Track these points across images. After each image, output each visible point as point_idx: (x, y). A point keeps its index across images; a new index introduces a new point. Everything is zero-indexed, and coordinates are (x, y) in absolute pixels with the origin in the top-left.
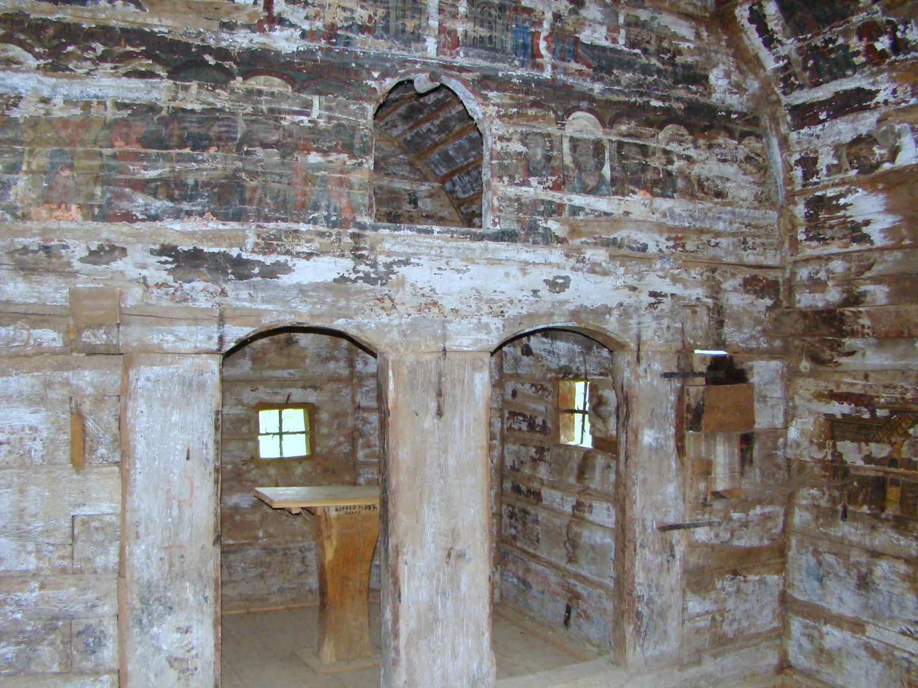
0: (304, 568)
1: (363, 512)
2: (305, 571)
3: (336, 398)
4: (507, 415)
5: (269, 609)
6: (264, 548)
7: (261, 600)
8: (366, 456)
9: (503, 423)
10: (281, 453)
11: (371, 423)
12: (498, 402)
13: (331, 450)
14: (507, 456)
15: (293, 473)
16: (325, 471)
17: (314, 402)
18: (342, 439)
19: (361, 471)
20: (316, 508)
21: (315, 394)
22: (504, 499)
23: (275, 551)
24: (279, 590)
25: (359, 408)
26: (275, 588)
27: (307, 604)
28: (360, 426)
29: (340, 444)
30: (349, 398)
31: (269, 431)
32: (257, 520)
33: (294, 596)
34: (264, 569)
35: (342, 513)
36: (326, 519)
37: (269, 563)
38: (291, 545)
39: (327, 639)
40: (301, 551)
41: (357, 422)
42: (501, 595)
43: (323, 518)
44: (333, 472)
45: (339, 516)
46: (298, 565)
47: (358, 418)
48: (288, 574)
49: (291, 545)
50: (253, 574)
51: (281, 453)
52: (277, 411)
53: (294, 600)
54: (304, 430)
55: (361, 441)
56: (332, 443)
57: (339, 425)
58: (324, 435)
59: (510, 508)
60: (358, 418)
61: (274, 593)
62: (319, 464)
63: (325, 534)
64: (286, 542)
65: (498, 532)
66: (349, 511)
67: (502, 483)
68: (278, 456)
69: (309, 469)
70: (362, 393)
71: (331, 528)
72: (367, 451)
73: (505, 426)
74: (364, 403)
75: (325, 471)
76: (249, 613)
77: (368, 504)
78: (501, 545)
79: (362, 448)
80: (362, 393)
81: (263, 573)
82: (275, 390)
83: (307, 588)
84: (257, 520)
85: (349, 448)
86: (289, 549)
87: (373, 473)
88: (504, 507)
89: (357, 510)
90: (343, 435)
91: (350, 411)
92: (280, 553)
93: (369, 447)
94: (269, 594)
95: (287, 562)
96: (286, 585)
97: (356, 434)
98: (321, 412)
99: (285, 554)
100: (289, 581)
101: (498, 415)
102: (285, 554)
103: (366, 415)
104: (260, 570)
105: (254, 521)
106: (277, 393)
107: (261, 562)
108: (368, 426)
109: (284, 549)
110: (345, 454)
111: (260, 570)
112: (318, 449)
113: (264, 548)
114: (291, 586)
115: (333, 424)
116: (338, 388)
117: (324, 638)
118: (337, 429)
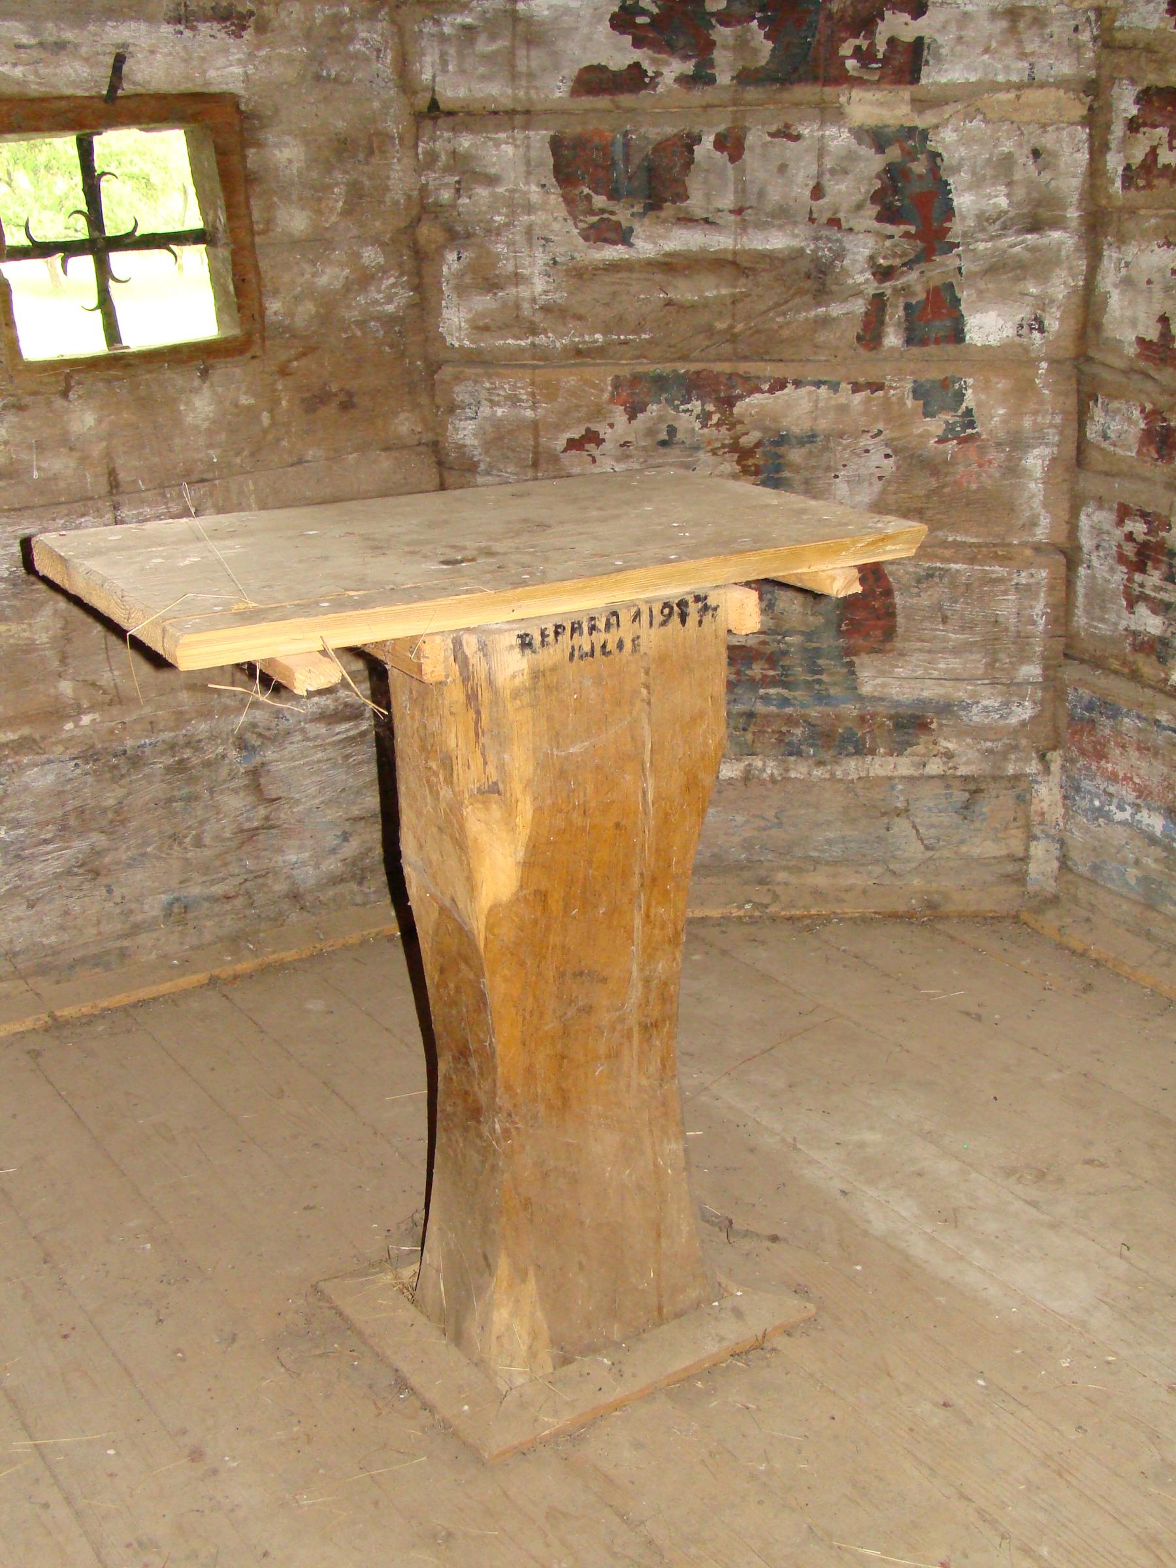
0: (262, 811)
1: (652, 637)
2: (268, 825)
3: (333, 69)
4: (1126, 105)
5: (144, 993)
6: (89, 755)
7: (97, 961)
8: (480, 328)
9: (1098, 149)
10: (112, 332)
11: (492, 180)
12: (1078, 48)
13: (328, 304)
14: (1116, 302)
15: (177, 420)
16: (315, 401)
17: (237, 87)
18: (371, 256)
19: (461, 393)
20: (412, 643)
21: (238, 50)
22: (1090, 484)
23: (136, 760)
24: (168, 910)
25: (434, 111)
26: (153, 907)
27: (289, 955)
28: (446, 196)
29: (365, 279)
30: (386, 65)
31: (105, 185)
32: (42, 638)
33: (230, 924)
34: (98, 839)
35: (556, 653)
36: (472, 698)
37: (119, 809)
38: (202, 728)
39: (503, 1266)
40: (242, 745)
41: (430, 178)
42: (1064, 862)
43: (455, 694)
44: (347, 406)
45: (537, 675)
46: (235, 803)
47: (433, 156)
48: (198, 843)
49: (202, 728)
50: (55, 866)
51: (112, 332)
52: (65, 145)
53: (235, 942)
54: (195, 222)
55: (451, 265)
56: (330, 276)
57: (356, 192)
58: (295, 243)
59: (1139, 528)
60: (433, 156)
61: (149, 926)
62: (284, 372)
63: (470, 776)
64: (181, 718)
65: (1053, 621)
66: (584, 641)
67: (1082, 416)
68: (95, 345)
69: (246, 400)
70: (443, 39)
71: (503, 741)
72: (483, 302)
73: (1114, 163)
74: (453, 91)
75: (315, 401)
76: (56, 1026)
77: (674, 591)
78: (1071, 672)
79: (462, 290)
80: (443, 39)
81: (96, 853)
82: (51, 31)
83: (280, 887)
84: (42, 638)
85: (404, 296)
86: (192, 743)
87: (514, 400)
88: (1092, 519)
89: (626, 631)
90: (377, 241)
91: (393, 129)
92: (161, 763)
93: (491, 285)
94: (135, 930)
95: (191, 799)
96: (195, 890)
97: (427, 232)
98: (270, 137)
99: (181, 767)
100: (205, 869)
101: (1079, 111)
102: (181, 767)
103: (465, 142)
104: (80, 846)
105: (29, 648)
106: (60, 46)
107: (80, 811)
108: (482, 192)
109: (172, 747)
110: (389, 321)
111: (80, 846)
112: (274, 307)
113: (89, 755)
114: (218, 889)
115: (328, 188)
116: (337, 20)
117: (488, 1265)
118: (347, 212)
